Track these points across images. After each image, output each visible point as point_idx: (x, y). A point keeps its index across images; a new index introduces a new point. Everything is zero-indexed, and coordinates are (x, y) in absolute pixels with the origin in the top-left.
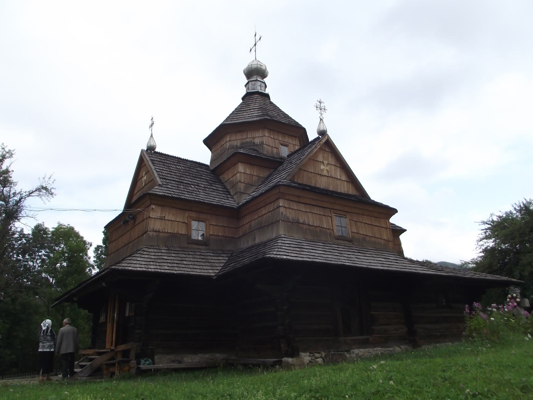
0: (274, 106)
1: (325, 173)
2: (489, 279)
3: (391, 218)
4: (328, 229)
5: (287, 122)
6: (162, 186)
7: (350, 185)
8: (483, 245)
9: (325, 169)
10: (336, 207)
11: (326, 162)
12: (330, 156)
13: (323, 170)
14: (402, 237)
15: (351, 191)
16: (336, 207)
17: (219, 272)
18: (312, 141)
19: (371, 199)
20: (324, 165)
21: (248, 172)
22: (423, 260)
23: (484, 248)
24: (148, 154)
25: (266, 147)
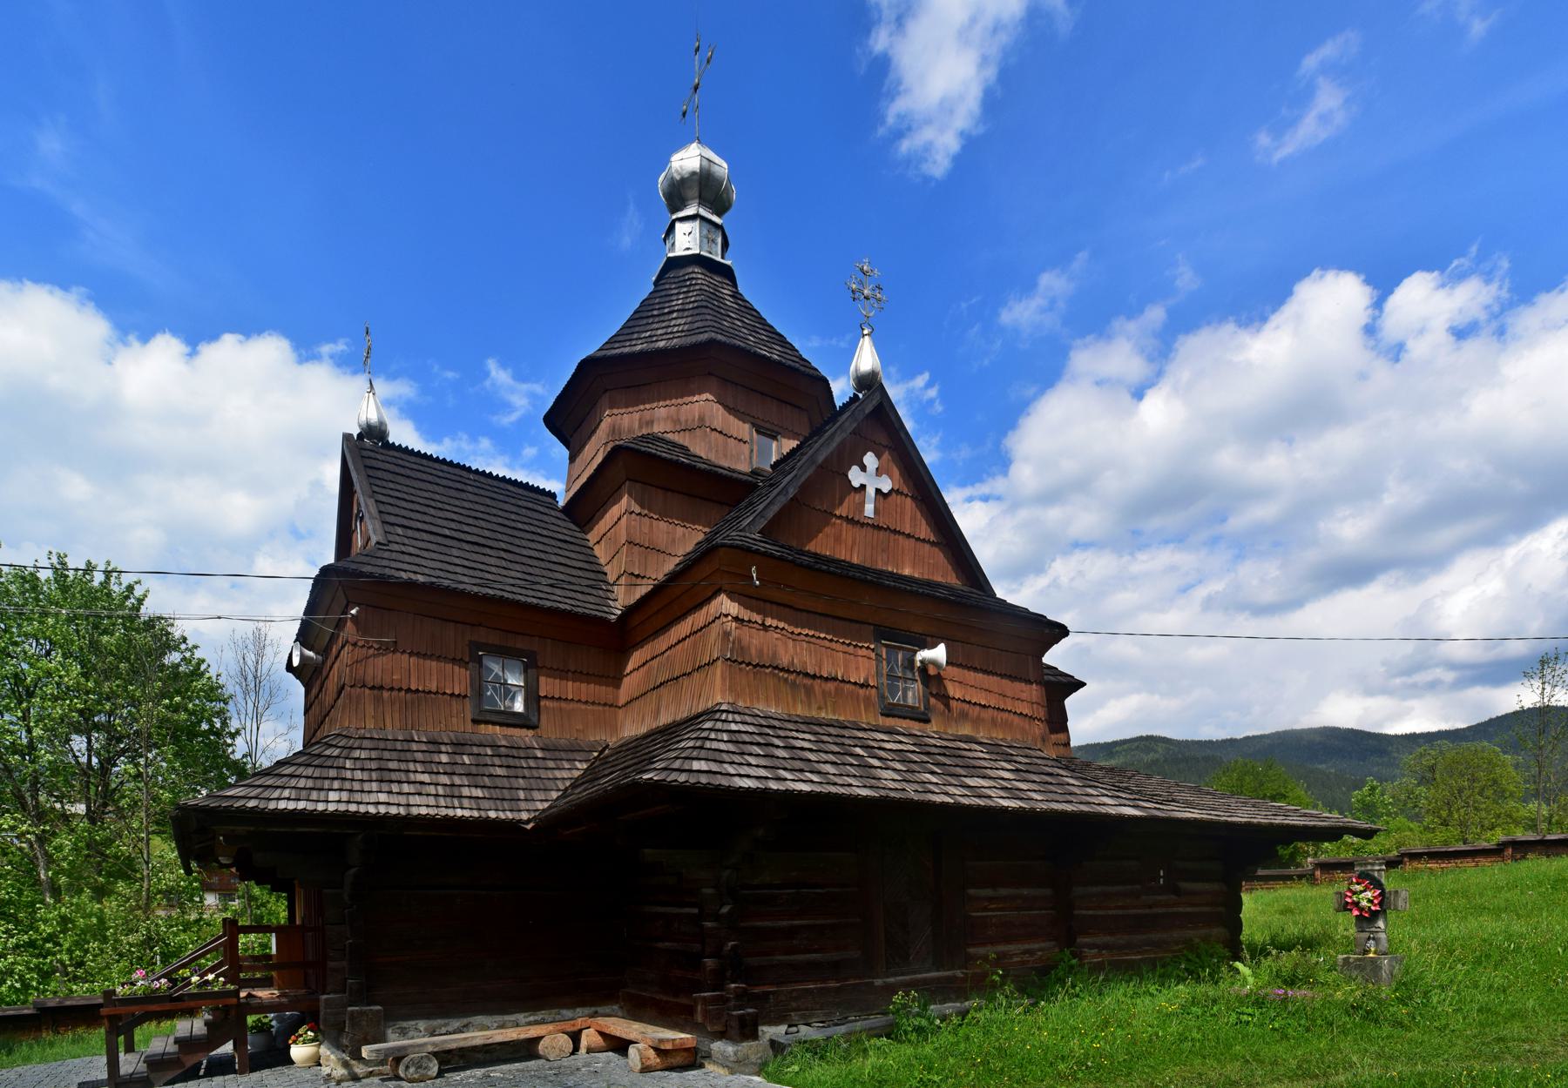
0: (745, 307)
2: (1294, 826)
3: (1063, 640)
5: (776, 357)
6: (385, 548)
14: (1071, 702)
15: (944, 574)
17: (550, 807)
18: (846, 406)
19: (997, 596)
24: (369, 476)
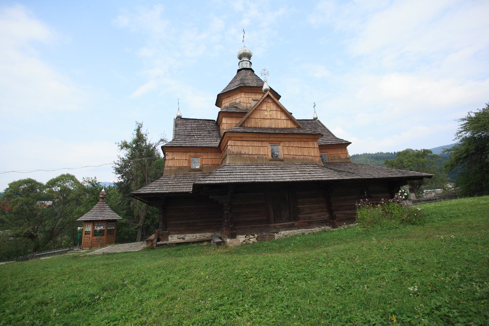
1: (268, 117)
4: (264, 155)
7: (289, 122)
8: (461, 136)
9: (268, 115)
10: (271, 139)
11: (269, 110)
12: (272, 105)
13: (266, 115)
16: (271, 139)
20: (267, 112)
21: (229, 122)
22: (421, 150)
23: (461, 138)
25: (242, 104)
